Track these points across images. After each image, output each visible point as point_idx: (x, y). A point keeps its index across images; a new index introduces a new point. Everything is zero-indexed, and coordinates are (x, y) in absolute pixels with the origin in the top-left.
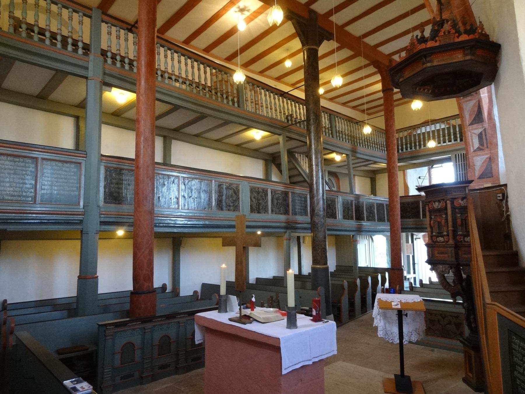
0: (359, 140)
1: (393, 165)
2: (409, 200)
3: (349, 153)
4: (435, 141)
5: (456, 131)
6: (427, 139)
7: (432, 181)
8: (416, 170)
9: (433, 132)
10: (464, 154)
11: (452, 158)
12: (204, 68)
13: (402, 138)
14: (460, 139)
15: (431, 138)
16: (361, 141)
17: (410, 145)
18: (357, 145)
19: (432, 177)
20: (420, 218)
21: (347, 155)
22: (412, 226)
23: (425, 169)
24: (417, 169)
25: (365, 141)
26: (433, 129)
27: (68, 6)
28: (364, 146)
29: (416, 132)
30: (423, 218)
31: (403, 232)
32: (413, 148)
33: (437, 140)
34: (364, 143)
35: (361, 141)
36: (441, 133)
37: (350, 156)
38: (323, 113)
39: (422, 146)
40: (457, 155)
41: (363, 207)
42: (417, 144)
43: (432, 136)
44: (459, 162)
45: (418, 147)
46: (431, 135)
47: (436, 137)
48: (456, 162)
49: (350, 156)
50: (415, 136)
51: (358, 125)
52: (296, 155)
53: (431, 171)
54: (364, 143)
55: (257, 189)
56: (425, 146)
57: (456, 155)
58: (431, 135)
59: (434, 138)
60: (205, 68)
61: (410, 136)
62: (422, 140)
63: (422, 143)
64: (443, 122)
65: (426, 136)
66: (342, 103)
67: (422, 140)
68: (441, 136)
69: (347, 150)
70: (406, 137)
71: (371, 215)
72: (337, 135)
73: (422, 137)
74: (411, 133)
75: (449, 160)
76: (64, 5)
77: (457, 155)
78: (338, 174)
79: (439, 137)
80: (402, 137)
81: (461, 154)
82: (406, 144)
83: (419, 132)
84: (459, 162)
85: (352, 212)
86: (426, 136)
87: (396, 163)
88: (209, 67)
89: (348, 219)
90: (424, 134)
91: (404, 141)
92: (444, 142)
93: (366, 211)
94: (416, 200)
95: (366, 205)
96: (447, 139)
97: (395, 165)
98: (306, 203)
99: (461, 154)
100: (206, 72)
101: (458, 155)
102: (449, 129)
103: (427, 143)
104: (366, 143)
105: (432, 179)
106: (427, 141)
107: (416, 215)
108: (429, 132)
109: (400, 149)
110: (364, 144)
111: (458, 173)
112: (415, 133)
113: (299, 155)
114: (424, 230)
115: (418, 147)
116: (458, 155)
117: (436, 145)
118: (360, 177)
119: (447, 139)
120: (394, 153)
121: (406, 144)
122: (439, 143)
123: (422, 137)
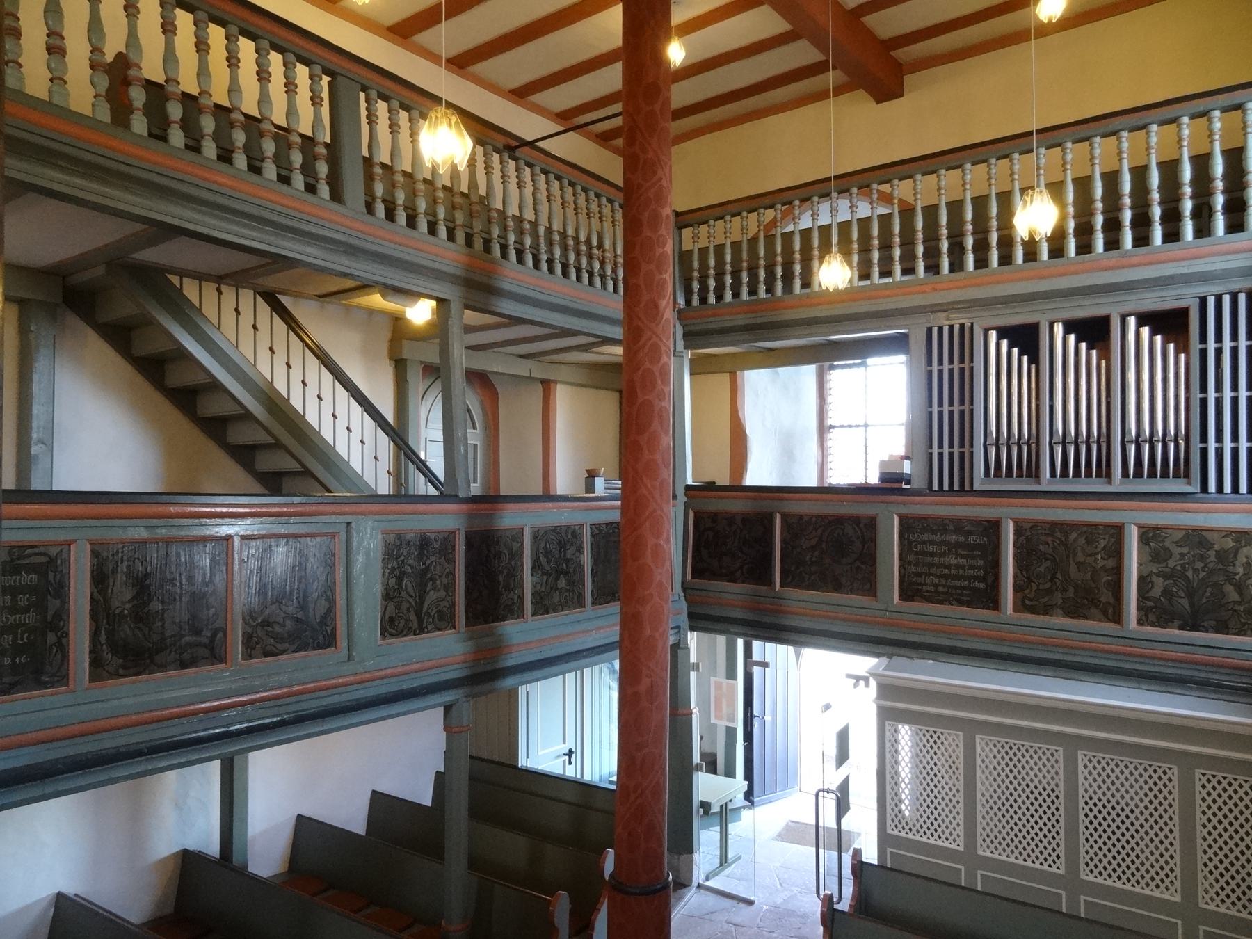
0: (520, 232)
1: (647, 365)
2: (737, 505)
3: (446, 291)
4: (850, 264)
5: (913, 231)
6: (816, 253)
7: (830, 414)
8: (777, 372)
9: (844, 227)
10: (962, 326)
11: (912, 341)
12: (285, 65)
13: (719, 249)
14: (1000, 258)
15: (835, 249)
16: (528, 242)
17: (749, 275)
18: (504, 255)
19: (829, 399)
20: (770, 583)
21: (440, 301)
22: (738, 614)
23: (807, 373)
24: (781, 370)
25: (550, 243)
26: (844, 216)
27: (227, 18)
28: (545, 266)
29: (814, 216)
30: (782, 586)
31: (692, 629)
32: (762, 288)
33: (855, 258)
34: (543, 248)
35: (528, 242)
36: (875, 232)
37: (455, 306)
38: (362, 95)
39: (798, 283)
40: (935, 331)
41: (517, 555)
42: (779, 271)
43: (839, 243)
44: (940, 362)
45: (779, 286)
46: (835, 239)
47: (855, 246)
48: (930, 363)
49: (455, 306)
50: (788, 237)
51: (516, 159)
52: (190, 290)
53: (828, 377)
54: (543, 248)
55: (1142, 567)
56: (806, 284)
57: (929, 330)
58: (835, 239)
59: (846, 253)
60: (264, 53)
61: (770, 240)
62: (797, 256)
63: (797, 269)
64: (864, 188)
65: (816, 243)
66: (510, 92)
67: (797, 256)
68: (876, 242)
69: (437, 275)
70: (753, 241)
71: (562, 583)
72: (369, 192)
73: (797, 246)
74: (774, 223)
75: (898, 344)
76: (277, 41)
77: (935, 331)
78: (494, 379)
79: (865, 250)
80: (724, 245)
81: (951, 328)
82: (736, 274)
83: (805, 222)
84: (940, 362)
85: (450, 588)
86: (816, 243)
87: (665, 359)
88: (307, 62)
89: (422, 630)
90: (806, 233)
91: (728, 258)
92: (886, 273)
93: (536, 566)
94: (764, 506)
95: (536, 538)
96: (897, 258)
97: (656, 369)
98: (53, 604)
99: (951, 328)
100: (395, 128)
101: (941, 329)
102: (907, 212)
103: (816, 270)
104: (557, 253)
105: (831, 407)
106: (816, 263)
107: (759, 572)
108: (825, 230)
109: (696, 290)
110: (544, 257)
111: (935, 409)
112: (790, 228)
113: (210, 289)
114: (786, 635)
115: (779, 286)
116: (941, 329)
117: (850, 281)
118: (579, 389)
119: (897, 258)
120: (656, 306)
121: (736, 274)
122: (865, 276)
123: (797, 246)
